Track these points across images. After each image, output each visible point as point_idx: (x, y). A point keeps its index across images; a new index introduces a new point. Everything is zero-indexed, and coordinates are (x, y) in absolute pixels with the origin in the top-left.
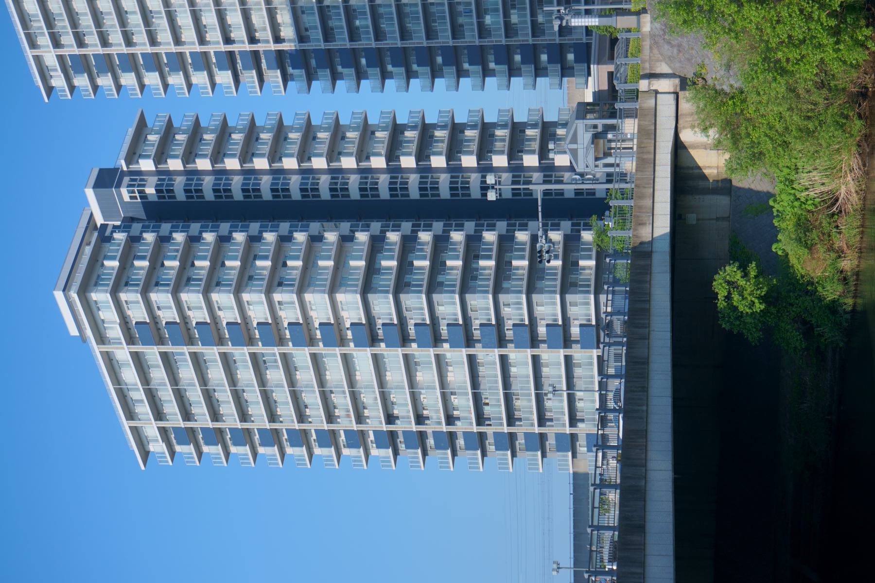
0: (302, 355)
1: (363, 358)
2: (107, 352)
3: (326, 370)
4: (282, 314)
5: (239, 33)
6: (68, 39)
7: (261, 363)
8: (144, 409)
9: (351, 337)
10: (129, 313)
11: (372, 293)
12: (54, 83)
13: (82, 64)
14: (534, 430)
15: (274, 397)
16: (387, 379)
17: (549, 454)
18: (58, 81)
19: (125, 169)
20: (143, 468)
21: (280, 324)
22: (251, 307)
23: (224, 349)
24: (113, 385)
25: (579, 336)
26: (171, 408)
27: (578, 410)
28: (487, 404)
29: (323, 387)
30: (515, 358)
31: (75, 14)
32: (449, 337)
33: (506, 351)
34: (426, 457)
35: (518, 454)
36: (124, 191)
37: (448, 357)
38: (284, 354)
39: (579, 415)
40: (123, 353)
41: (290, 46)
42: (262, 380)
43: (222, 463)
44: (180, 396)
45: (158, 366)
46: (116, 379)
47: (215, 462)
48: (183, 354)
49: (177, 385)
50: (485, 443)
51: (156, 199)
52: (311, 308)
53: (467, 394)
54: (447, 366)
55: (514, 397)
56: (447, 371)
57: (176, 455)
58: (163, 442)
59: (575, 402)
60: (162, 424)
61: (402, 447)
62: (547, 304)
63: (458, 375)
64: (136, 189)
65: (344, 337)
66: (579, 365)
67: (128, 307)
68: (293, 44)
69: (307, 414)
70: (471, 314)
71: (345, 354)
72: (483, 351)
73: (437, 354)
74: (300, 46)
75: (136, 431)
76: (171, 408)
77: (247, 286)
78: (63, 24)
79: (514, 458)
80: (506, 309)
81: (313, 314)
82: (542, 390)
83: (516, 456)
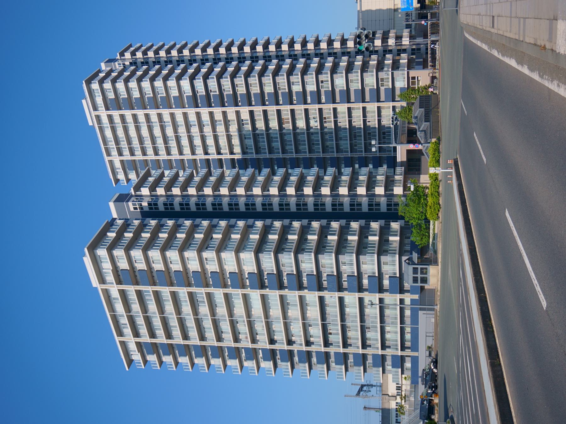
2: (106, 289)
3: (252, 308)
4: (207, 267)
5: (280, 336)
8: (128, 331)
10: (119, 264)
11: (404, 256)
13: (155, 348)
15: (273, 328)
16: (289, 315)
17: (350, 369)
18: (136, 357)
21: (243, 275)
23: (227, 291)
24: (109, 312)
25: (388, 286)
26: (143, 330)
27: (387, 340)
28: (331, 334)
29: (267, 319)
30: (348, 302)
32: (369, 287)
33: (343, 294)
34: (312, 370)
35: (349, 369)
37: (366, 302)
38: (227, 294)
39: (387, 343)
43: (221, 371)
44: (182, 322)
46: (112, 309)
47: (234, 372)
48: (148, 292)
49: (130, 312)
50: (347, 361)
51: (148, 210)
52: (225, 263)
53: (318, 325)
54: (307, 306)
55: (367, 330)
56: (307, 310)
57: (260, 369)
59: (346, 332)
60: (138, 340)
61: (333, 365)
63: (313, 313)
65: (226, 284)
67: (207, 262)
69: (257, 339)
71: (245, 294)
72: (328, 294)
73: (301, 296)
76: (143, 330)
78: (124, 144)
79: (365, 373)
80: (343, 266)
81: (226, 267)
82: (365, 323)
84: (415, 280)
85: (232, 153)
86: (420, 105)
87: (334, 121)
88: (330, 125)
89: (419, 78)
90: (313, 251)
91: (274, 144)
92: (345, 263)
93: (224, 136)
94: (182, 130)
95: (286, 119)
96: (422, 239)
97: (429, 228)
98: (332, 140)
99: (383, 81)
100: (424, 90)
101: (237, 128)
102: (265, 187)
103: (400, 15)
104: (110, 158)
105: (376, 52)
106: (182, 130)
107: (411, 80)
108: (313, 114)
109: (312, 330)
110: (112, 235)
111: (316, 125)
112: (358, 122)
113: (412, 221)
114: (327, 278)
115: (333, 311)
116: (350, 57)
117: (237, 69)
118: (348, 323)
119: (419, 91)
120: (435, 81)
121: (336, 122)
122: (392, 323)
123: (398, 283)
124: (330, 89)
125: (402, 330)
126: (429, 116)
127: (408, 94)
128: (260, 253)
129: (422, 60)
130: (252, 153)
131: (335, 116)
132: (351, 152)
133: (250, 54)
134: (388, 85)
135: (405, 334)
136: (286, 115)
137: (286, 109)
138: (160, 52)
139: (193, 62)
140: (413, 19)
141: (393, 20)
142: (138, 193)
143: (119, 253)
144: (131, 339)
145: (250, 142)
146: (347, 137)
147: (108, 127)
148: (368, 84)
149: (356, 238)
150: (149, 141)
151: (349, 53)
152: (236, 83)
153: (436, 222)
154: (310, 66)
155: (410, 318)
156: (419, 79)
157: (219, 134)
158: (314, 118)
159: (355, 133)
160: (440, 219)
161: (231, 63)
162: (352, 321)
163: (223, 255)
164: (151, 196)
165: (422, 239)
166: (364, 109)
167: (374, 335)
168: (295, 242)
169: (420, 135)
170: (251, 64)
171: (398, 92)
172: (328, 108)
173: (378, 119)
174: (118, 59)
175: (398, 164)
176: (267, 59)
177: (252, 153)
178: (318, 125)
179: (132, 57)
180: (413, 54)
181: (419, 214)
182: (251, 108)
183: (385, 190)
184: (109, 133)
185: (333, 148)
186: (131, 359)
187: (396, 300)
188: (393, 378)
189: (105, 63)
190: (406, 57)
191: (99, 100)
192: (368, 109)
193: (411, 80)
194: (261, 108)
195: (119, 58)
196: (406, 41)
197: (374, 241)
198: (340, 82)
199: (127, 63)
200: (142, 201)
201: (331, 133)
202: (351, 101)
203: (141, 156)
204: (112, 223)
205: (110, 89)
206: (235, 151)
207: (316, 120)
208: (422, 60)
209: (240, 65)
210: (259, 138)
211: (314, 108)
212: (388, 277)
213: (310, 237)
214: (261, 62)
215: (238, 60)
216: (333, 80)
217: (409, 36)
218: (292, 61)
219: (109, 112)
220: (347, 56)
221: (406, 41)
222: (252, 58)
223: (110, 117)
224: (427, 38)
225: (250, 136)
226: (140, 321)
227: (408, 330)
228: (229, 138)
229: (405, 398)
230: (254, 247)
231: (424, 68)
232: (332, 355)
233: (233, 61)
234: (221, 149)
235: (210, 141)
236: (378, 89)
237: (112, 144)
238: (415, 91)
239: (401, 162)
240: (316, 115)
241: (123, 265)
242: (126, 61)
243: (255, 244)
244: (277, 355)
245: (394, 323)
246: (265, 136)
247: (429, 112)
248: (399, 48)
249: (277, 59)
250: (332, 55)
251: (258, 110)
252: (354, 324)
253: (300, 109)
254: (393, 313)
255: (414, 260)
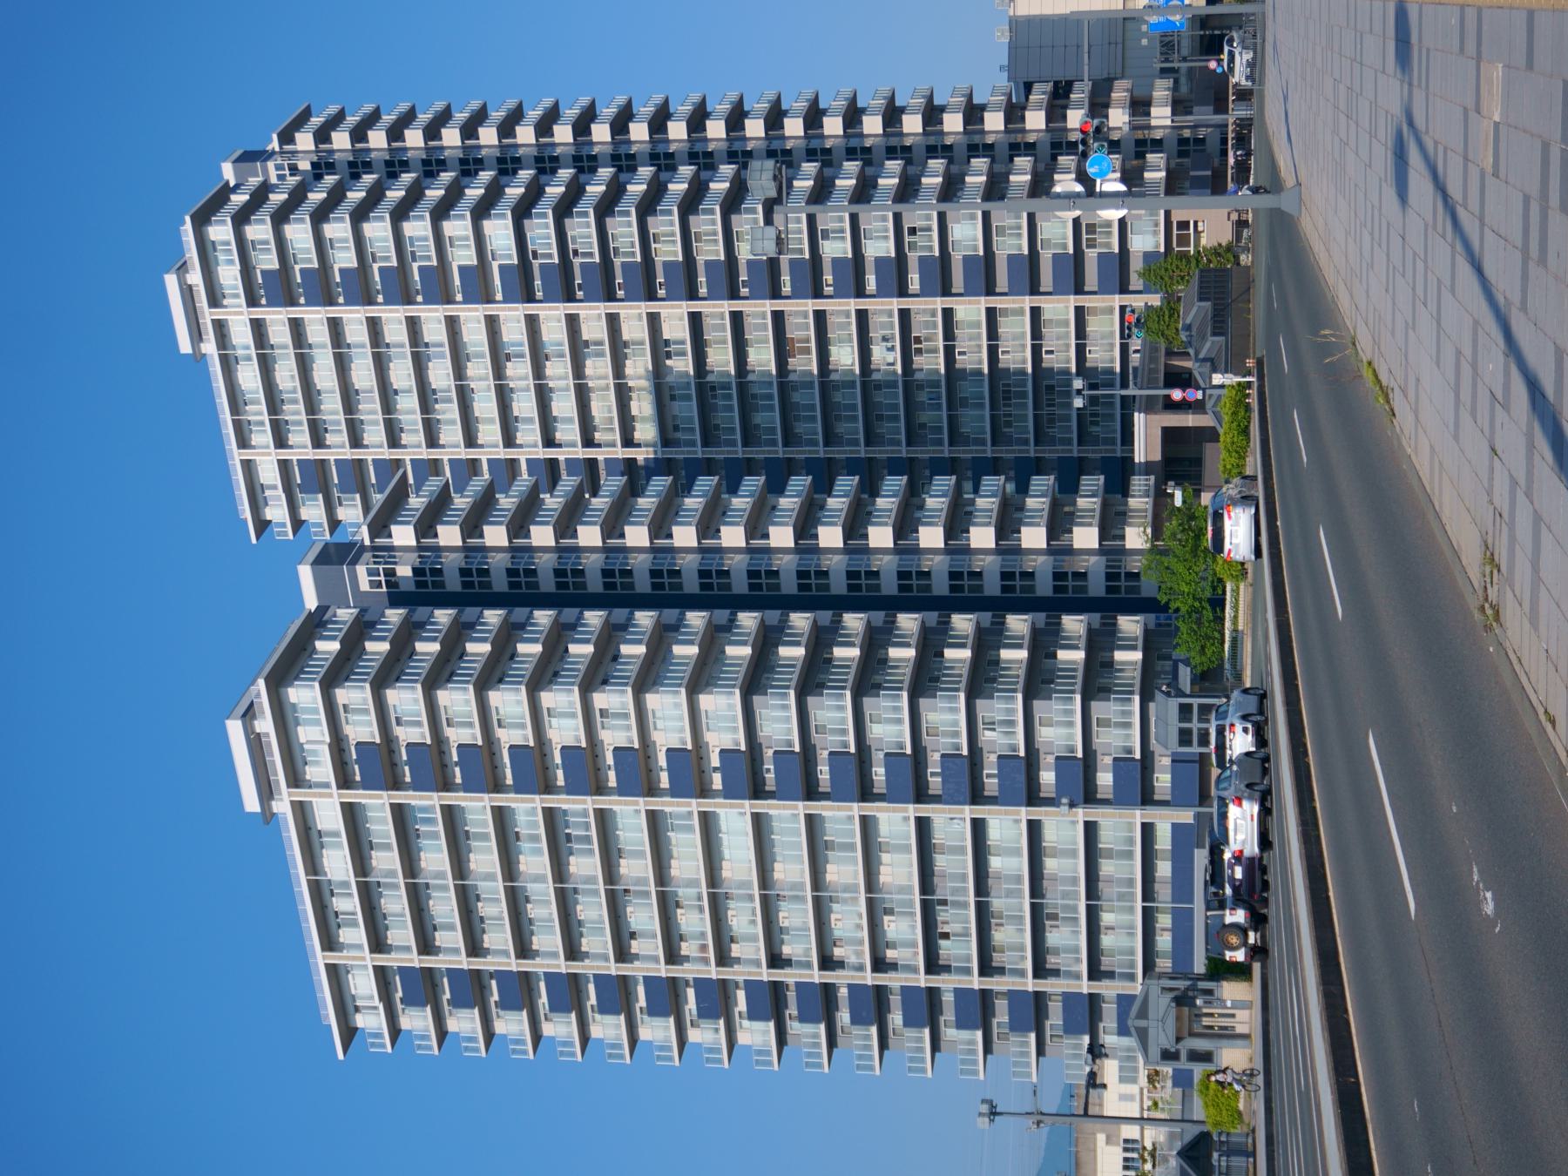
0: (630, 815)
1: (734, 819)
6: (401, 933)
7: (563, 839)
9: (720, 787)
12: (360, 1021)
13: (423, 987)
14: (1026, 984)
17: (997, 1044)
18: (371, 1021)
19: (367, 542)
20: (341, 1056)
22: (554, 721)
28: (946, 936)
30: (998, 837)
31: (315, 393)
36: (361, 570)
40: (328, 815)
41: (647, 453)
42: (559, 870)
45: (387, 847)
51: (412, 588)
55: (1048, 923)
58: (380, 1000)
62: (1059, 724)
63: (899, 870)
64: (381, 567)
66: (1110, 854)
68: (651, 449)
70: (926, 740)
74: (663, 453)
75: (334, 971)
76: (401, 933)
77: (550, 682)
78: (295, 412)
80: (987, 733)
83: (991, 1053)
84: (1185, 737)
85: (628, 442)
86: (1200, 293)
87: (946, 347)
88: (932, 362)
89: (1200, 224)
90: (906, 685)
91: (759, 418)
92: (993, 723)
93: (607, 388)
94: (479, 370)
95: (800, 341)
96: (1203, 648)
97: (1222, 619)
98: (939, 406)
99: (1094, 233)
100: (1213, 258)
101: (650, 368)
102: (756, 526)
103: (1145, 42)
104: (247, 454)
105: (1030, 148)
106: (479, 370)
107: (1176, 231)
108: (883, 326)
109: (892, 925)
110: (328, 647)
111: (891, 360)
112: (1016, 356)
113: (1178, 604)
114: (942, 767)
115: (955, 865)
116: (951, 161)
117: (575, 193)
118: (997, 903)
119: (1198, 261)
120: (1246, 233)
121: (950, 353)
122: (1121, 897)
123: (1139, 776)
124: (937, 254)
125: (1148, 917)
126: (1223, 322)
127: (1166, 270)
128: (755, 694)
129: (1209, 173)
130: (692, 443)
131: (949, 334)
132: (993, 445)
133: (573, 148)
134: (1108, 245)
135: (1154, 934)
136: (801, 329)
137: (800, 312)
138: (334, 135)
139: (360, 170)
140: (1185, 52)
141: (1120, 46)
142: (380, 541)
143: (355, 695)
144: (363, 959)
145: (688, 410)
146: (983, 398)
147: (249, 358)
148: (1049, 240)
149: (1023, 654)
150: (374, 403)
151: (948, 149)
152: (652, 231)
153: (1242, 586)
154: (875, 186)
155: (1169, 886)
156: (1200, 229)
157: (591, 384)
158: (885, 339)
159: (1009, 385)
160: (1250, 575)
161: (476, 173)
162: (1009, 894)
163: (652, 700)
164: (420, 548)
165: (1203, 648)
166: (1036, 312)
167: (1067, 938)
168: (855, 665)
169: (1200, 370)
170: (575, 179)
171: (1136, 265)
172: (927, 308)
173: (1077, 345)
174: (273, 153)
175: (1137, 468)
176: (624, 163)
177: (692, 443)
178: (895, 359)
179: (316, 147)
180: (1181, 154)
181: (1197, 583)
182: (696, 306)
183: (1102, 538)
184: (249, 377)
185: (939, 430)
186: (352, 1025)
187: (1131, 826)
188: (1121, 1069)
189: (234, 162)
190: (1162, 164)
191: (229, 275)
192: (1046, 316)
193: (1175, 232)
194: (726, 306)
195: (277, 149)
196: (1161, 116)
197: (1074, 662)
198: (966, 233)
199: (304, 165)
200: (395, 563)
201: (936, 384)
202: (998, 290)
203: (347, 449)
204: (316, 623)
205: (266, 242)
206: (638, 435)
207: (889, 345)
208: (1209, 173)
209: (543, 179)
210: (714, 397)
211: (885, 309)
212: (1111, 762)
213: (893, 652)
214: (605, 172)
215: (496, 166)
216: (946, 227)
217: (1170, 101)
218: (821, 168)
219: (258, 313)
220: (943, 158)
221: (1161, 116)
222: (577, 159)
223: (258, 327)
224: (1226, 111)
225: (689, 389)
226: (395, 904)
227: (1164, 921)
228: (623, 395)
229: (1153, 1155)
230: (741, 676)
231: (1214, 193)
232: (948, 998)
233: (483, 170)
234: (595, 429)
235: (564, 406)
236: (1079, 255)
237: (257, 411)
238: (1189, 262)
239: (1147, 463)
240: (892, 328)
241: (361, 729)
242: (302, 159)
243: (743, 670)
244: (786, 1007)
245: (1128, 897)
246: (734, 392)
247: (1223, 310)
248: (1140, 135)
249: (690, 164)
250: (899, 155)
251: (717, 311)
252: (1012, 903)
253: (841, 309)
254: (1121, 870)
255: (1181, 686)
